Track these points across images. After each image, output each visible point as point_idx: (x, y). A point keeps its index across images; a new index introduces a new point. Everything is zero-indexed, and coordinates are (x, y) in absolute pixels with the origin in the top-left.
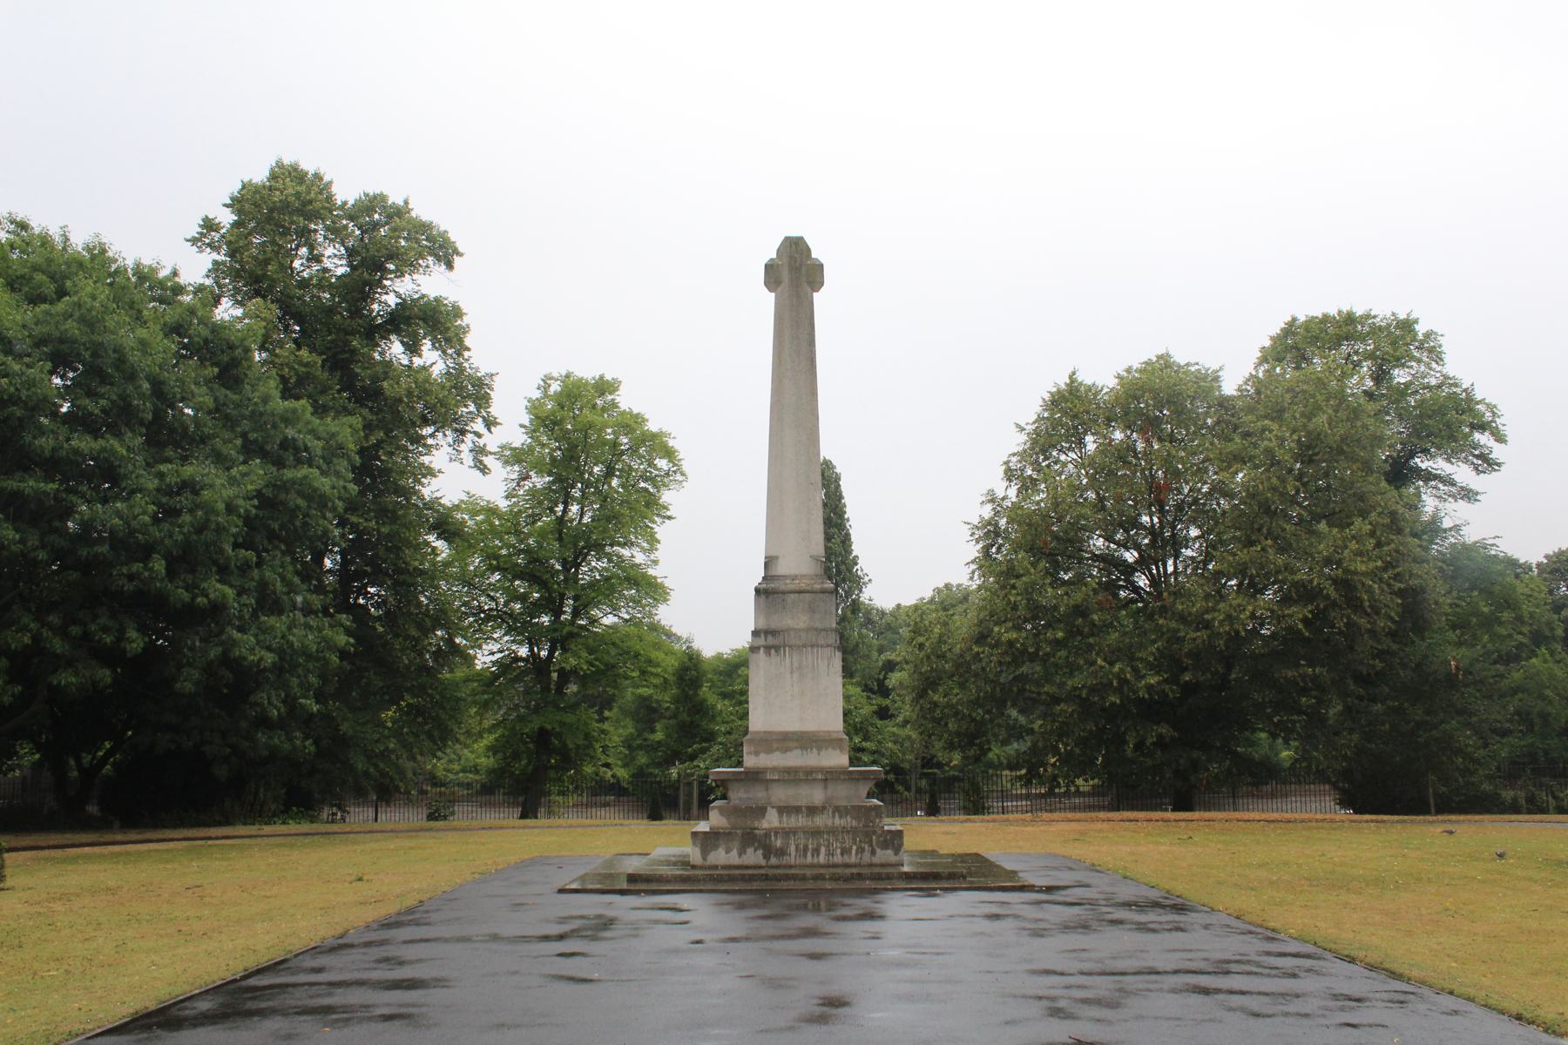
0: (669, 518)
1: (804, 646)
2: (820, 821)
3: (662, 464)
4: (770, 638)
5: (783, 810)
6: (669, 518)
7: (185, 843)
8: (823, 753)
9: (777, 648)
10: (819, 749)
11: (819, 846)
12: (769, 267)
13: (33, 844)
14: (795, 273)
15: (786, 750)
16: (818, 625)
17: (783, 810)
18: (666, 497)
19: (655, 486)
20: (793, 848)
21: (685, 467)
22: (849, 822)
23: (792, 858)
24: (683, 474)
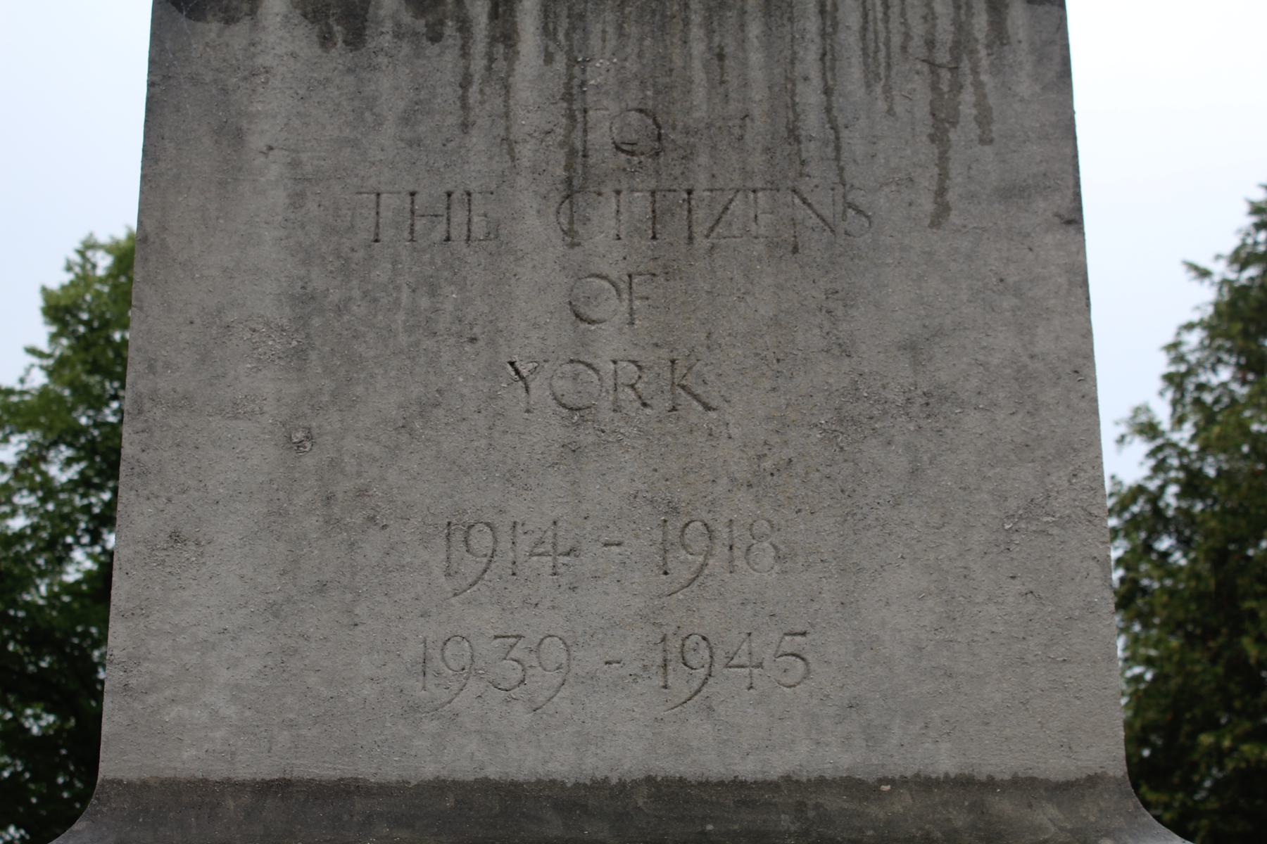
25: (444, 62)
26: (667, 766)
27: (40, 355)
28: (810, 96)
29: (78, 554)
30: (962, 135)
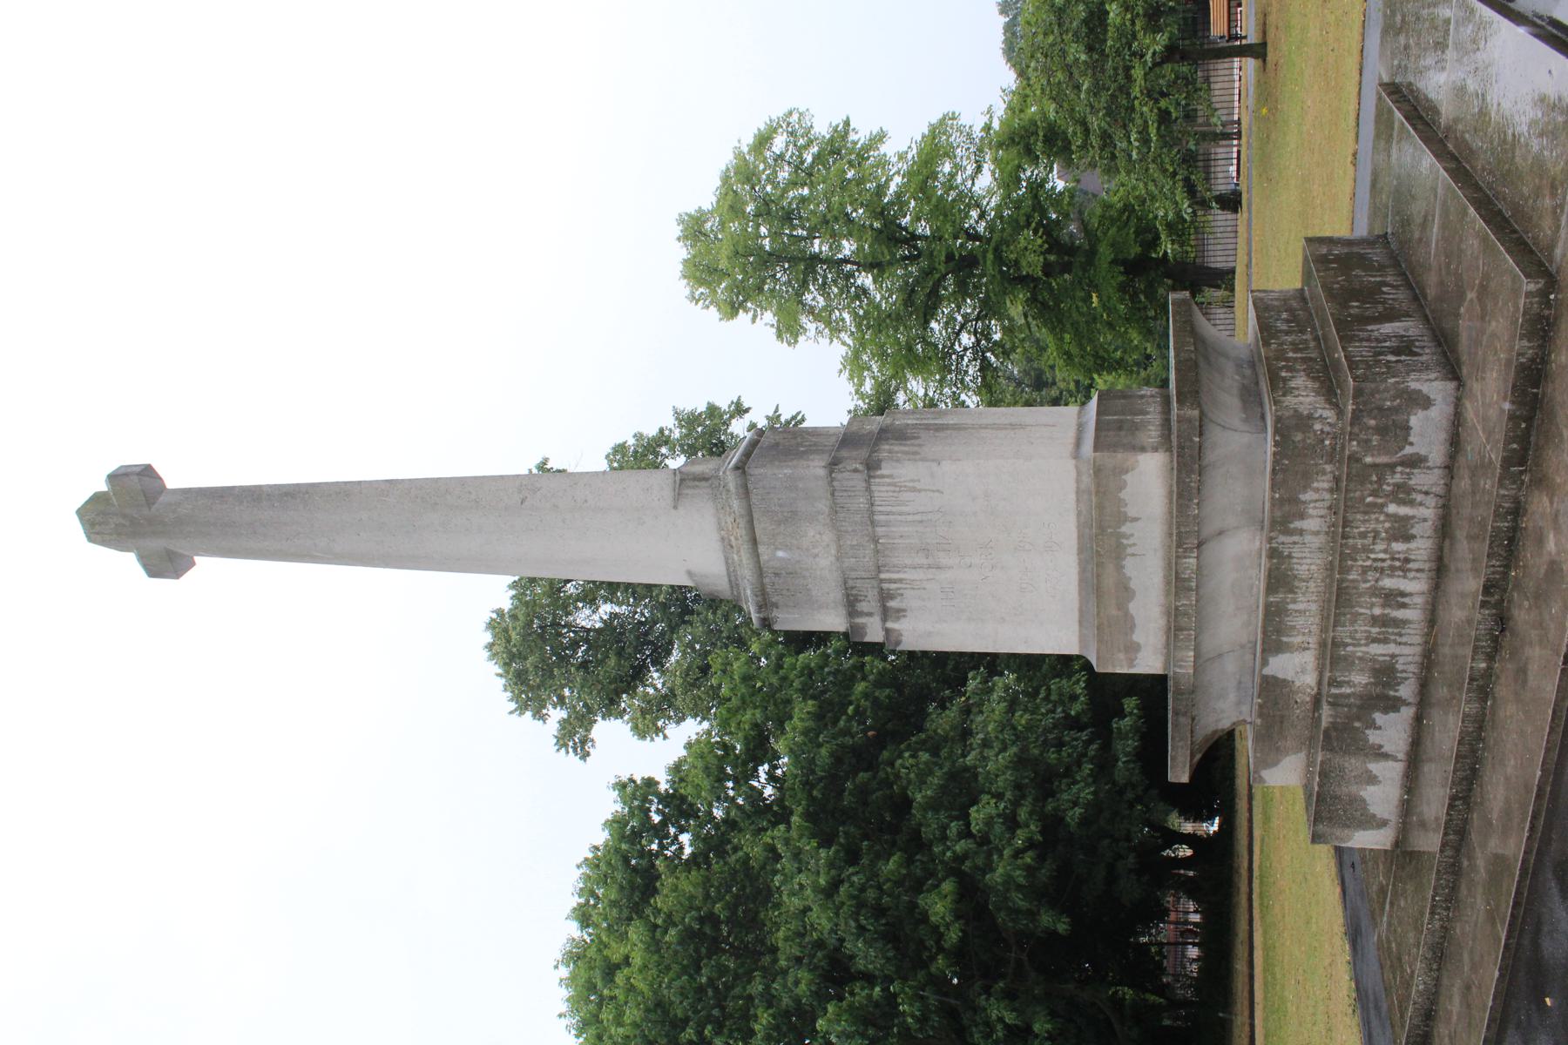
2: (1309, 559)
3: (779, 143)
4: (863, 606)
5: (1273, 637)
7: (1258, 1014)
8: (1131, 511)
10: (1123, 519)
11: (1375, 591)
12: (154, 571)
13: (1246, 1003)
14: (144, 518)
15: (1125, 591)
16: (823, 505)
17: (1273, 637)
18: (822, 129)
19: (810, 143)
20: (1376, 649)
21: (778, 112)
22: (1317, 498)
23: (1406, 652)
24: (790, 113)
25: (907, 593)
26: (1075, 550)
27: (755, 317)
28: (910, 518)
29: (859, 282)
30: (917, 485)
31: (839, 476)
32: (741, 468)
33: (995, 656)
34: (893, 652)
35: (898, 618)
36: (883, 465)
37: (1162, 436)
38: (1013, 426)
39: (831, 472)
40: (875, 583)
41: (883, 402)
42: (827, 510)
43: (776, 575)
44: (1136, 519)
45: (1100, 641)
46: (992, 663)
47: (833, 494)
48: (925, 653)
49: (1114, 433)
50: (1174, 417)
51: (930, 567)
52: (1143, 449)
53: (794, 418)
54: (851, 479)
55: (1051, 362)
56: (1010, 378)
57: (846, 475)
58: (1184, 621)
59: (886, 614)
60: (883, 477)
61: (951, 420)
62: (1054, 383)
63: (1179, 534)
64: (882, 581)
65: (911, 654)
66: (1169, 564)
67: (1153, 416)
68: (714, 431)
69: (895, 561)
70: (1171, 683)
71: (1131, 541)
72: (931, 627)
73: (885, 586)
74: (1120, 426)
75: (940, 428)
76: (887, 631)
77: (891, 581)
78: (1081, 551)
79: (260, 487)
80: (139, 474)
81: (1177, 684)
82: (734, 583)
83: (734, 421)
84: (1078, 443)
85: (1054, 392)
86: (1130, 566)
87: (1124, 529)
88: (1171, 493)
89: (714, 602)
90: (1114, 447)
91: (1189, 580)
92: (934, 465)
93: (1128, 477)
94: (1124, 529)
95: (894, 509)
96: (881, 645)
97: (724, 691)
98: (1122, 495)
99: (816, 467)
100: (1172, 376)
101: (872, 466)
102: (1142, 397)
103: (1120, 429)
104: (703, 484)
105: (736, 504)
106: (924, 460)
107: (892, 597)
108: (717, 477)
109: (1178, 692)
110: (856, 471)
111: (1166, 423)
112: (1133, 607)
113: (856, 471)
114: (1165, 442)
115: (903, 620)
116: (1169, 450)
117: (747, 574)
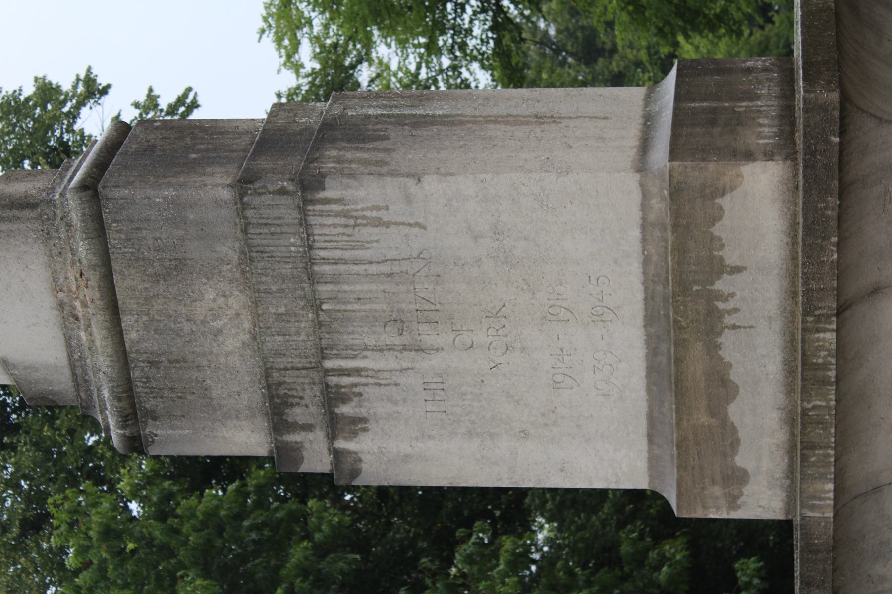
0: (20, 90)
1: (316, 305)
4: (298, 414)
6: (20, 90)
8: (731, 257)
9: (332, 397)
10: (719, 268)
15: (722, 387)
16: (229, 250)
25: (369, 392)
26: (640, 321)
28: (373, 269)
31: (256, 201)
32: (91, 187)
33: (521, 493)
34: (351, 489)
35: (354, 434)
36: (328, 182)
37: (780, 134)
38: (539, 119)
39: (241, 196)
40: (316, 376)
41: (335, 78)
42: (235, 257)
43: (151, 363)
44: (738, 270)
45: (682, 467)
46: (509, 508)
47: (245, 231)
48: (406, 492)
49: (704, 132)
50: (800, 104)
51: (405, 348)
52: (749, 156)
53: (181, 101)
54: (276, 207)
55: (609, 17)
56: (544, 40)
57: (267, 199)
58: (816, 434)
59: (335, 426)
60: (327, 201)
61: (438, 109)
62: (614, 50)
63: (807, 292)
64: (327, 372)
65: (383, 492)
66: (792, 341)
67: (767, 102)
68: (44, 127)
69: (349, 339)
70: (797, 534)
71: (731, 305)
72: (414, 443)
73: (333, 380)
74: (712, 119)
75: (420, 122)
76: (337, 454)
77: (342, 372)
78: (649, 320)
79: (216, 120)
80: (788, 36)
81: (806, 535)
82: (80, 380)
83: (84, 111)
84: (645, 145)
85: (615, 66)
86: (730, 346)
87: (718, 285)
88: (793, 225)
89: (48, 408)
90: (703, 153)
91: (825, 366)
92: (411, 182)
93: (725, 202)
94: (718, 285)
95: (347, 255)
96: (327, 478)
97: (71, 559)
98: (716, 230)
99: (217, 187)
100: (798, 38)
101: (309, 184)
102: (749, 70)
103: (712, 123)
104: (27, 213)
105: (83, 248)
106: (393, 174)
107: (344, 399)
108: (50, 203)
109: (809, 549)
110: (282, 192)
111: (787, 114)
112: (734, 411)
113: (282, 192)
114: (784, 147)
115: (362, 436)
116: (791, 157)
117: (102, 362)
